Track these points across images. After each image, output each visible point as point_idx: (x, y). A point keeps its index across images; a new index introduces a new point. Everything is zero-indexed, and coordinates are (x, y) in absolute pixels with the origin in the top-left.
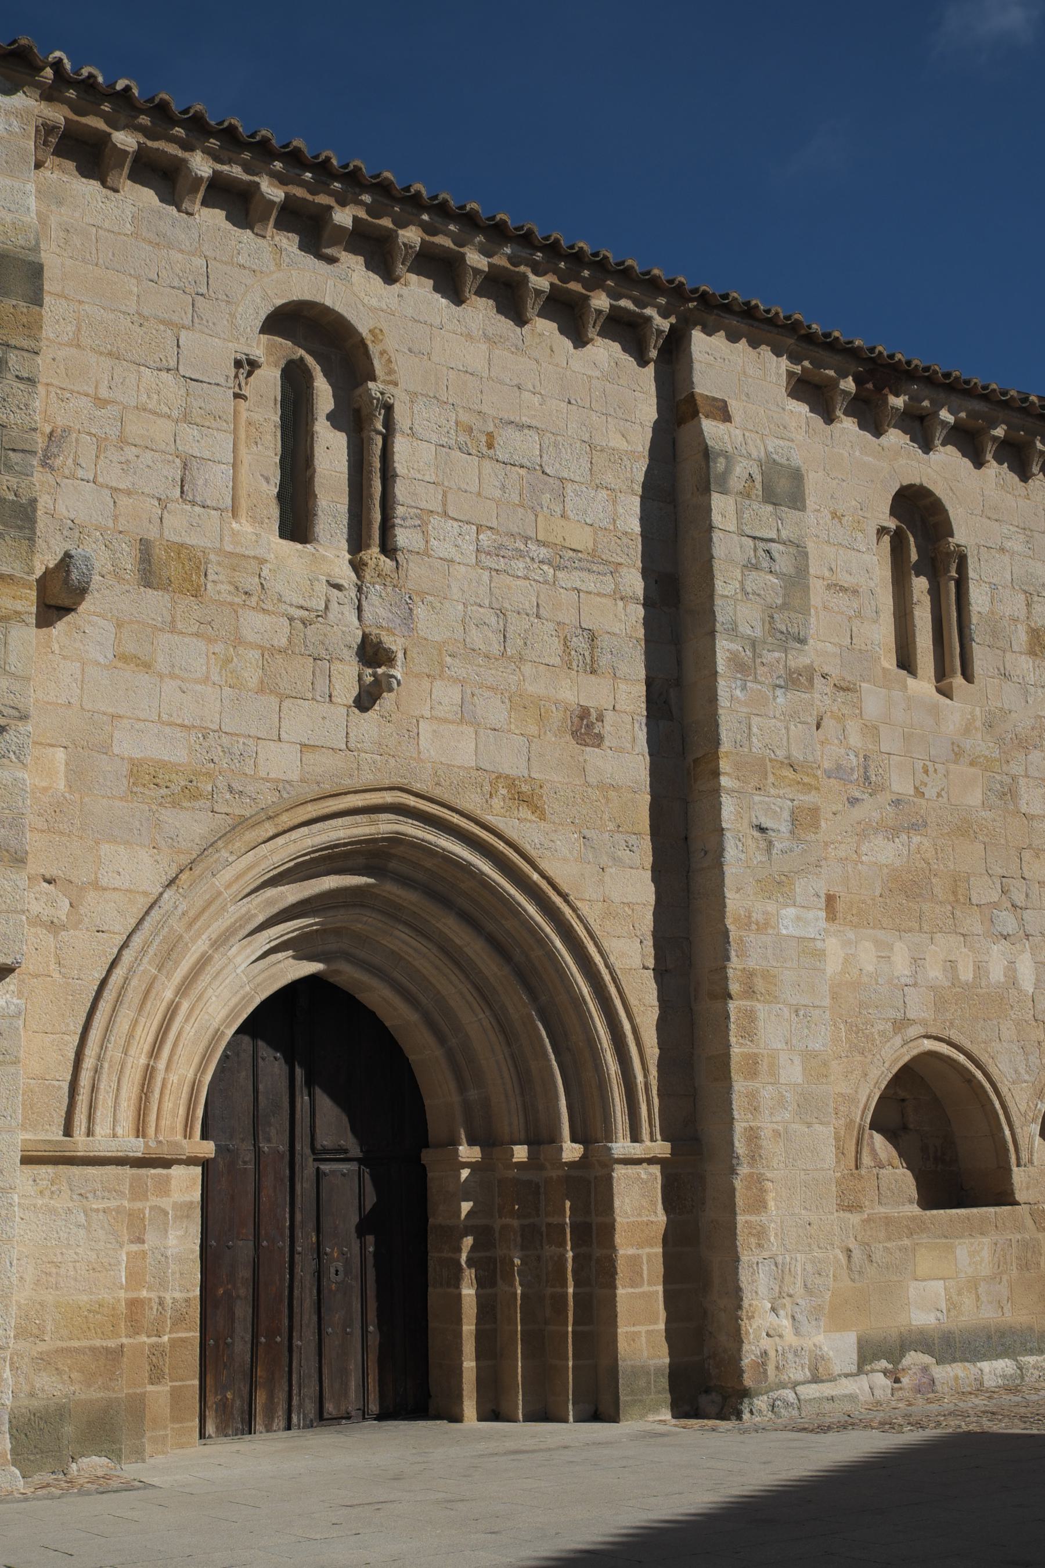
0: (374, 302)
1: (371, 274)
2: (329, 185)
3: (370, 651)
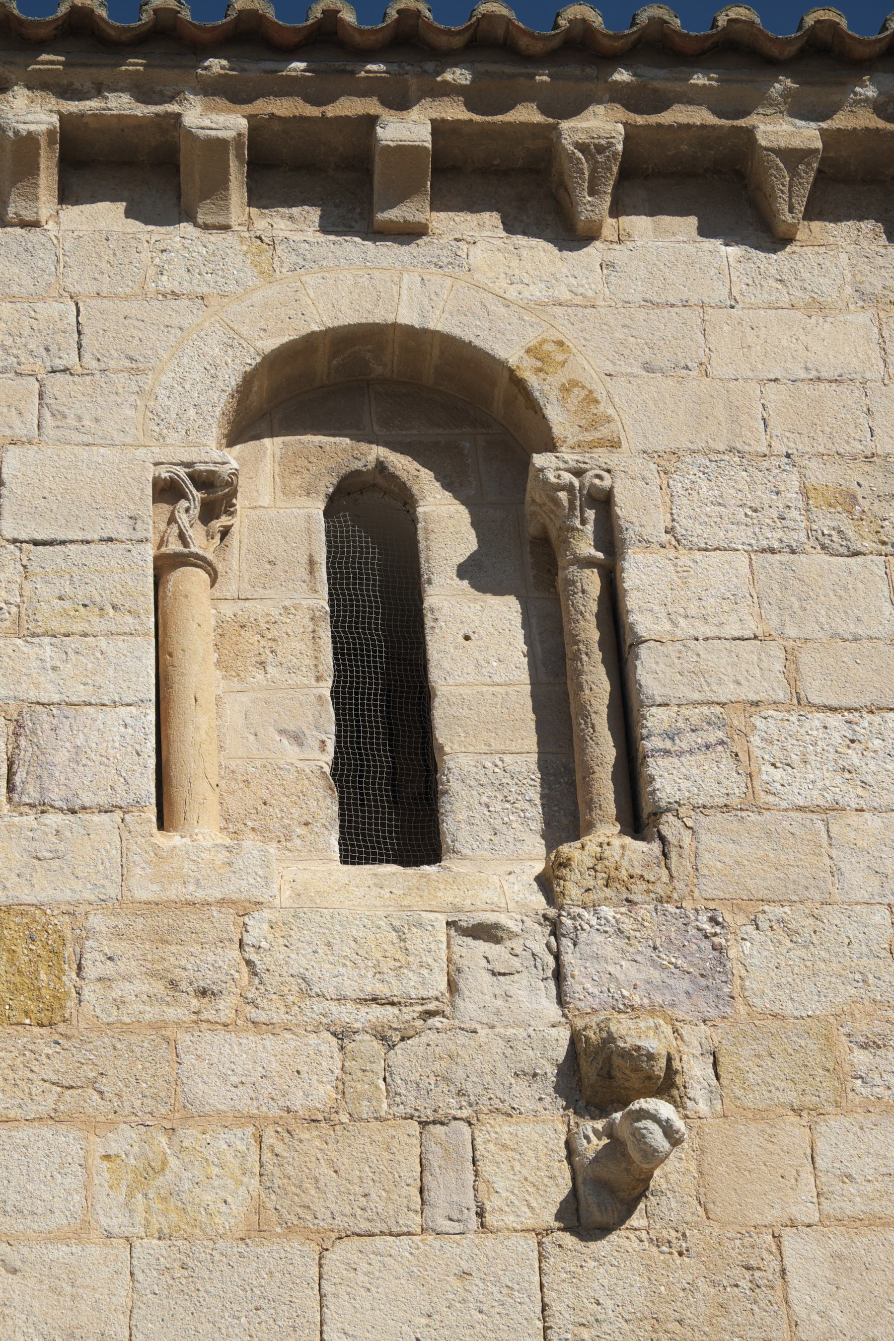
0: (537, 292)
1: (520, 240)
2: (353, 73)
3: (589, 1071)
